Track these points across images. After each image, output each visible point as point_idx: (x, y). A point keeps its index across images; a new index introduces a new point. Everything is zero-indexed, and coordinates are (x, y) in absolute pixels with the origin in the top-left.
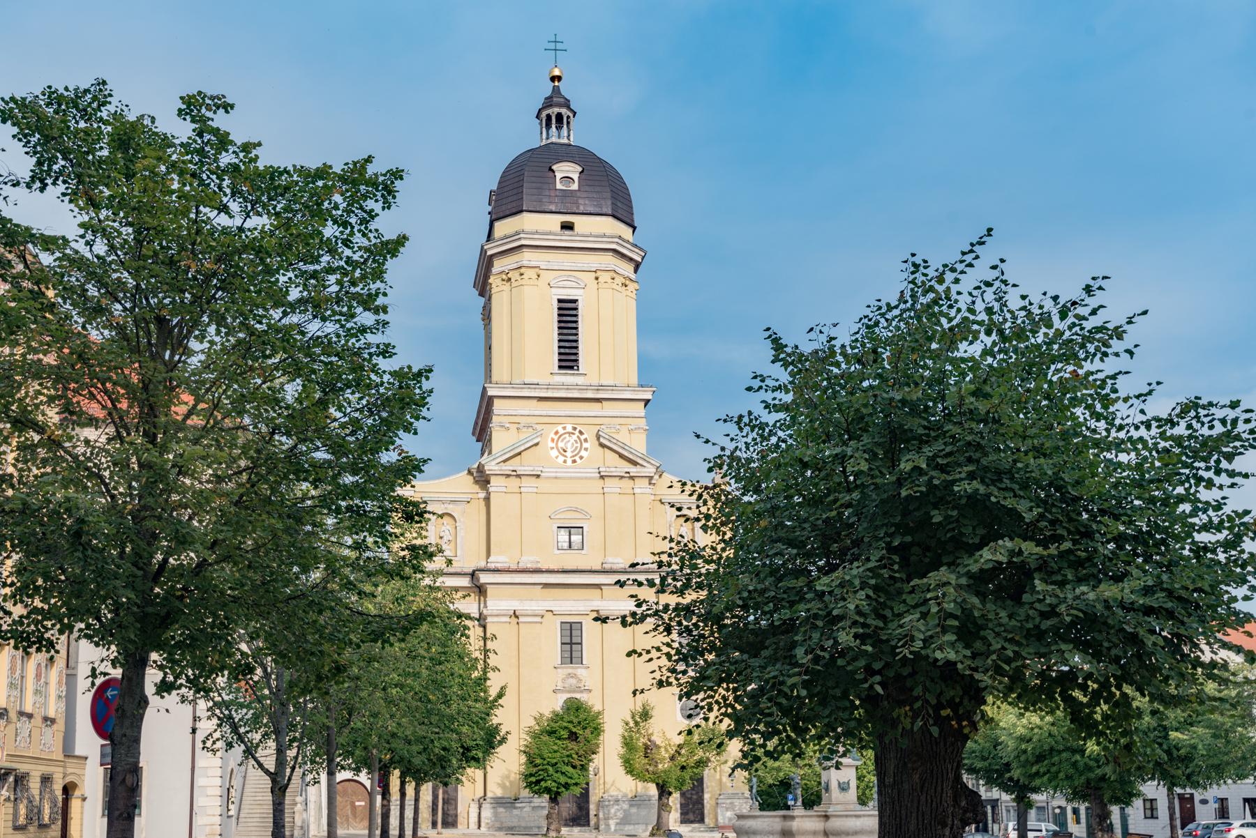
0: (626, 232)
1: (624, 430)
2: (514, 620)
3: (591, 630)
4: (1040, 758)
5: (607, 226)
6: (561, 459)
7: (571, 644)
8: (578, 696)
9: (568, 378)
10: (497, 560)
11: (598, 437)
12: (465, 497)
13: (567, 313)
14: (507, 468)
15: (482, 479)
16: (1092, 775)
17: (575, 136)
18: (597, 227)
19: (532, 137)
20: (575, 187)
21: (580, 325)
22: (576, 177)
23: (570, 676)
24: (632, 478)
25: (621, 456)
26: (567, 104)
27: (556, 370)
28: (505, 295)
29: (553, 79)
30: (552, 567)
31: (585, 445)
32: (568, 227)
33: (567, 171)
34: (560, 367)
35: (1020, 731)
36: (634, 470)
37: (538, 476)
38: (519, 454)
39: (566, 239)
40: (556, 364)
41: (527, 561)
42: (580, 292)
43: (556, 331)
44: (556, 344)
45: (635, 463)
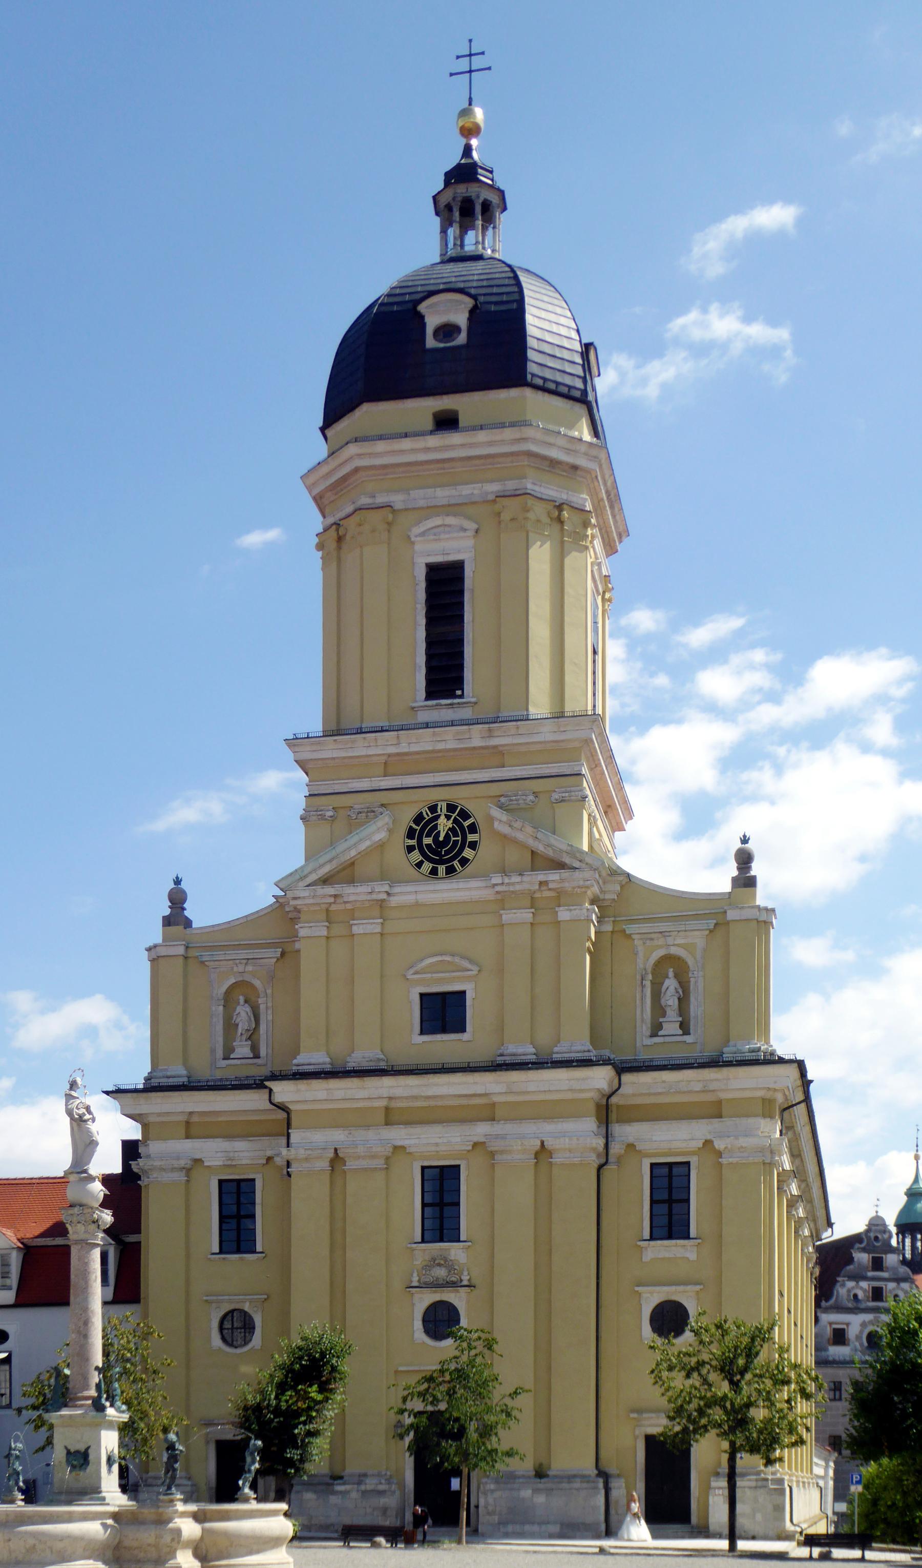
8: (449, 1296)
32: (446, 422)
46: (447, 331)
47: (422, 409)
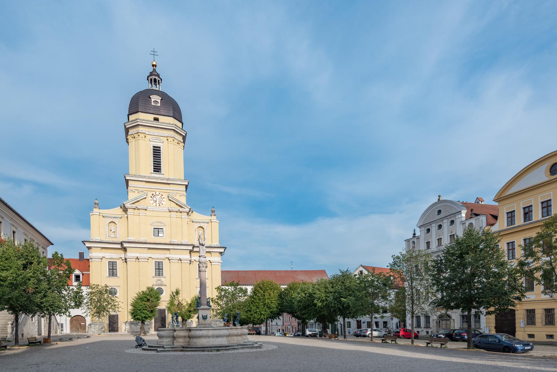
0: (180, 125)
1: (178, 195)
2: (180, 262)
3: (166, 264)
4: (305, 308)
5: (171, 120)
6: (155, 204)
7: (113, 269)
9: (157, 175)
10: (131, 239)
11: (168, 197)
12: (120, 216)
13: (157, 151)
14: (134, 206)
15: (125, 210)
16: (321, 314)
17: (161, 88)
18: (167, 120)
19: (147, 86)
20: (159, 105)
21: (161, 156)
22: (159, 101)
23: (160, 280)
24: (181, 212)
25: (177, 204)
26: (158, 75)
27: (152, 172)
28: (133, 143)
29: (153, 65)
30: (151, 242)
31: (164, 200)
32: (156, 119)
33: (155, 98)
34: (154, 171)
35: (298, 299)
36: (181, 209)
37: (146, 210)
38: (139, 201)
39: (155, 124)
40: (153, 170)
41: (142, 239)
42: (161, 144)
43: (152, 158)
44: (152, 162)
45: (182, 207)
46: (156, 102)
47: (151, 117)
